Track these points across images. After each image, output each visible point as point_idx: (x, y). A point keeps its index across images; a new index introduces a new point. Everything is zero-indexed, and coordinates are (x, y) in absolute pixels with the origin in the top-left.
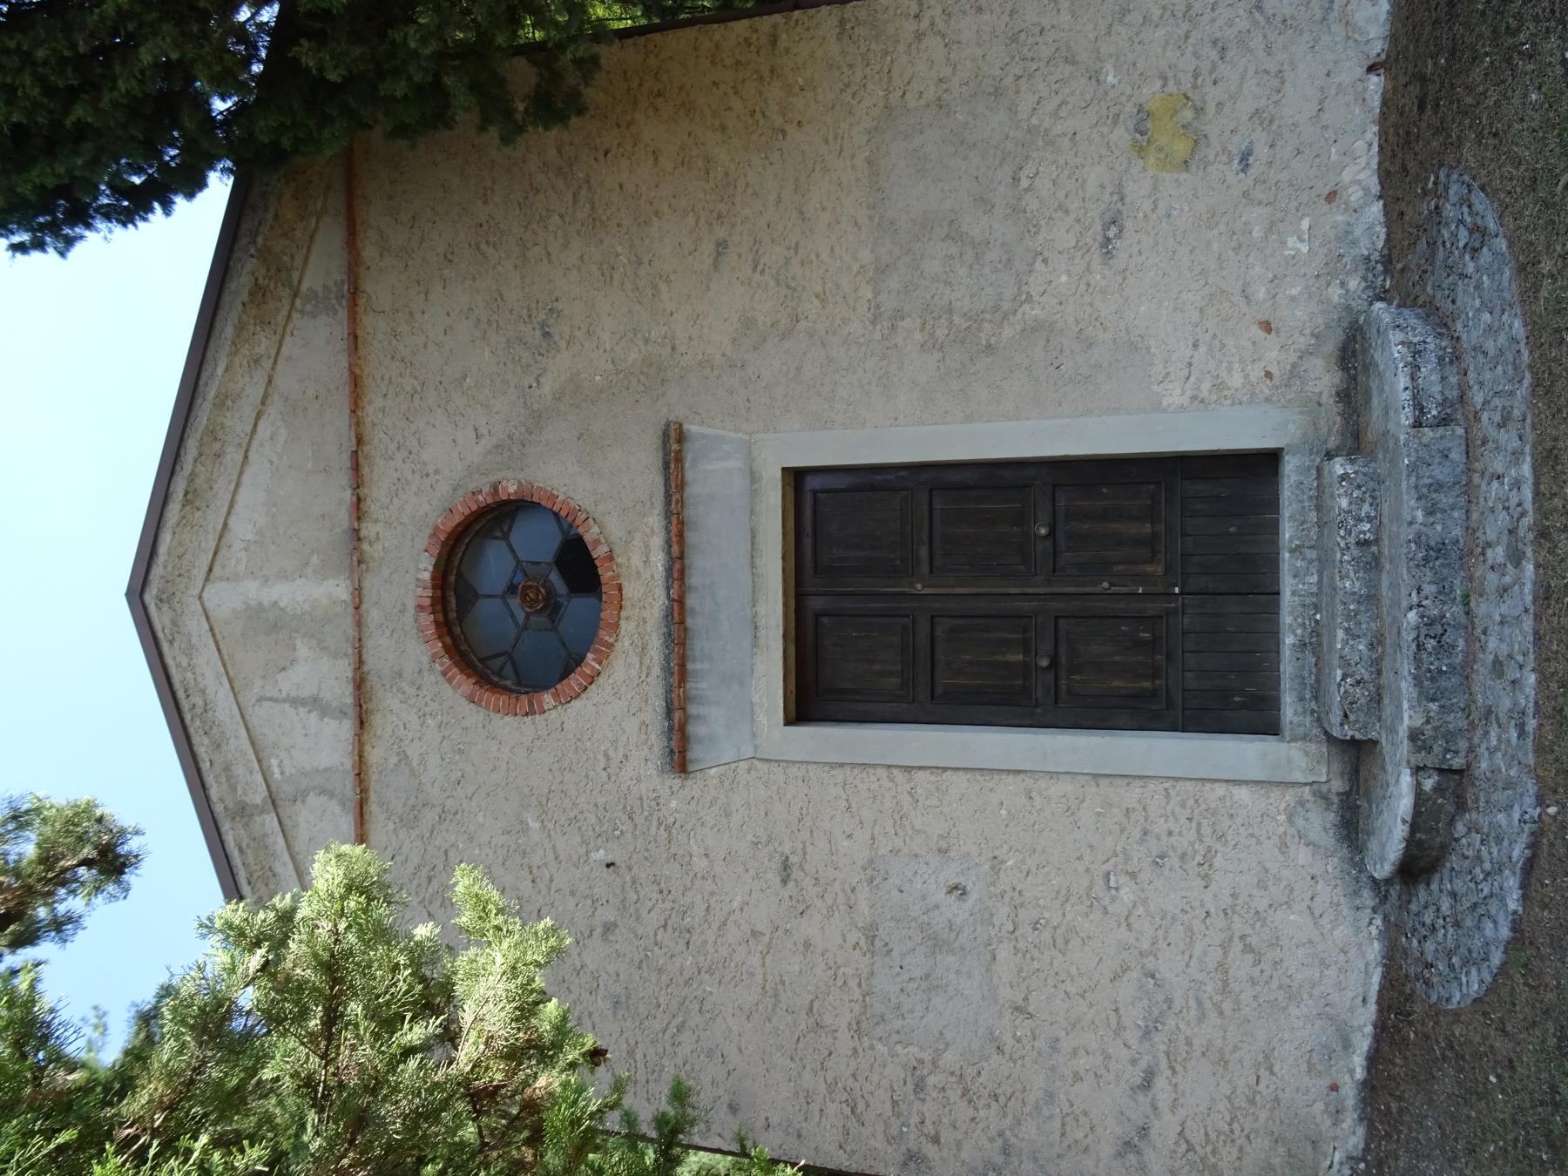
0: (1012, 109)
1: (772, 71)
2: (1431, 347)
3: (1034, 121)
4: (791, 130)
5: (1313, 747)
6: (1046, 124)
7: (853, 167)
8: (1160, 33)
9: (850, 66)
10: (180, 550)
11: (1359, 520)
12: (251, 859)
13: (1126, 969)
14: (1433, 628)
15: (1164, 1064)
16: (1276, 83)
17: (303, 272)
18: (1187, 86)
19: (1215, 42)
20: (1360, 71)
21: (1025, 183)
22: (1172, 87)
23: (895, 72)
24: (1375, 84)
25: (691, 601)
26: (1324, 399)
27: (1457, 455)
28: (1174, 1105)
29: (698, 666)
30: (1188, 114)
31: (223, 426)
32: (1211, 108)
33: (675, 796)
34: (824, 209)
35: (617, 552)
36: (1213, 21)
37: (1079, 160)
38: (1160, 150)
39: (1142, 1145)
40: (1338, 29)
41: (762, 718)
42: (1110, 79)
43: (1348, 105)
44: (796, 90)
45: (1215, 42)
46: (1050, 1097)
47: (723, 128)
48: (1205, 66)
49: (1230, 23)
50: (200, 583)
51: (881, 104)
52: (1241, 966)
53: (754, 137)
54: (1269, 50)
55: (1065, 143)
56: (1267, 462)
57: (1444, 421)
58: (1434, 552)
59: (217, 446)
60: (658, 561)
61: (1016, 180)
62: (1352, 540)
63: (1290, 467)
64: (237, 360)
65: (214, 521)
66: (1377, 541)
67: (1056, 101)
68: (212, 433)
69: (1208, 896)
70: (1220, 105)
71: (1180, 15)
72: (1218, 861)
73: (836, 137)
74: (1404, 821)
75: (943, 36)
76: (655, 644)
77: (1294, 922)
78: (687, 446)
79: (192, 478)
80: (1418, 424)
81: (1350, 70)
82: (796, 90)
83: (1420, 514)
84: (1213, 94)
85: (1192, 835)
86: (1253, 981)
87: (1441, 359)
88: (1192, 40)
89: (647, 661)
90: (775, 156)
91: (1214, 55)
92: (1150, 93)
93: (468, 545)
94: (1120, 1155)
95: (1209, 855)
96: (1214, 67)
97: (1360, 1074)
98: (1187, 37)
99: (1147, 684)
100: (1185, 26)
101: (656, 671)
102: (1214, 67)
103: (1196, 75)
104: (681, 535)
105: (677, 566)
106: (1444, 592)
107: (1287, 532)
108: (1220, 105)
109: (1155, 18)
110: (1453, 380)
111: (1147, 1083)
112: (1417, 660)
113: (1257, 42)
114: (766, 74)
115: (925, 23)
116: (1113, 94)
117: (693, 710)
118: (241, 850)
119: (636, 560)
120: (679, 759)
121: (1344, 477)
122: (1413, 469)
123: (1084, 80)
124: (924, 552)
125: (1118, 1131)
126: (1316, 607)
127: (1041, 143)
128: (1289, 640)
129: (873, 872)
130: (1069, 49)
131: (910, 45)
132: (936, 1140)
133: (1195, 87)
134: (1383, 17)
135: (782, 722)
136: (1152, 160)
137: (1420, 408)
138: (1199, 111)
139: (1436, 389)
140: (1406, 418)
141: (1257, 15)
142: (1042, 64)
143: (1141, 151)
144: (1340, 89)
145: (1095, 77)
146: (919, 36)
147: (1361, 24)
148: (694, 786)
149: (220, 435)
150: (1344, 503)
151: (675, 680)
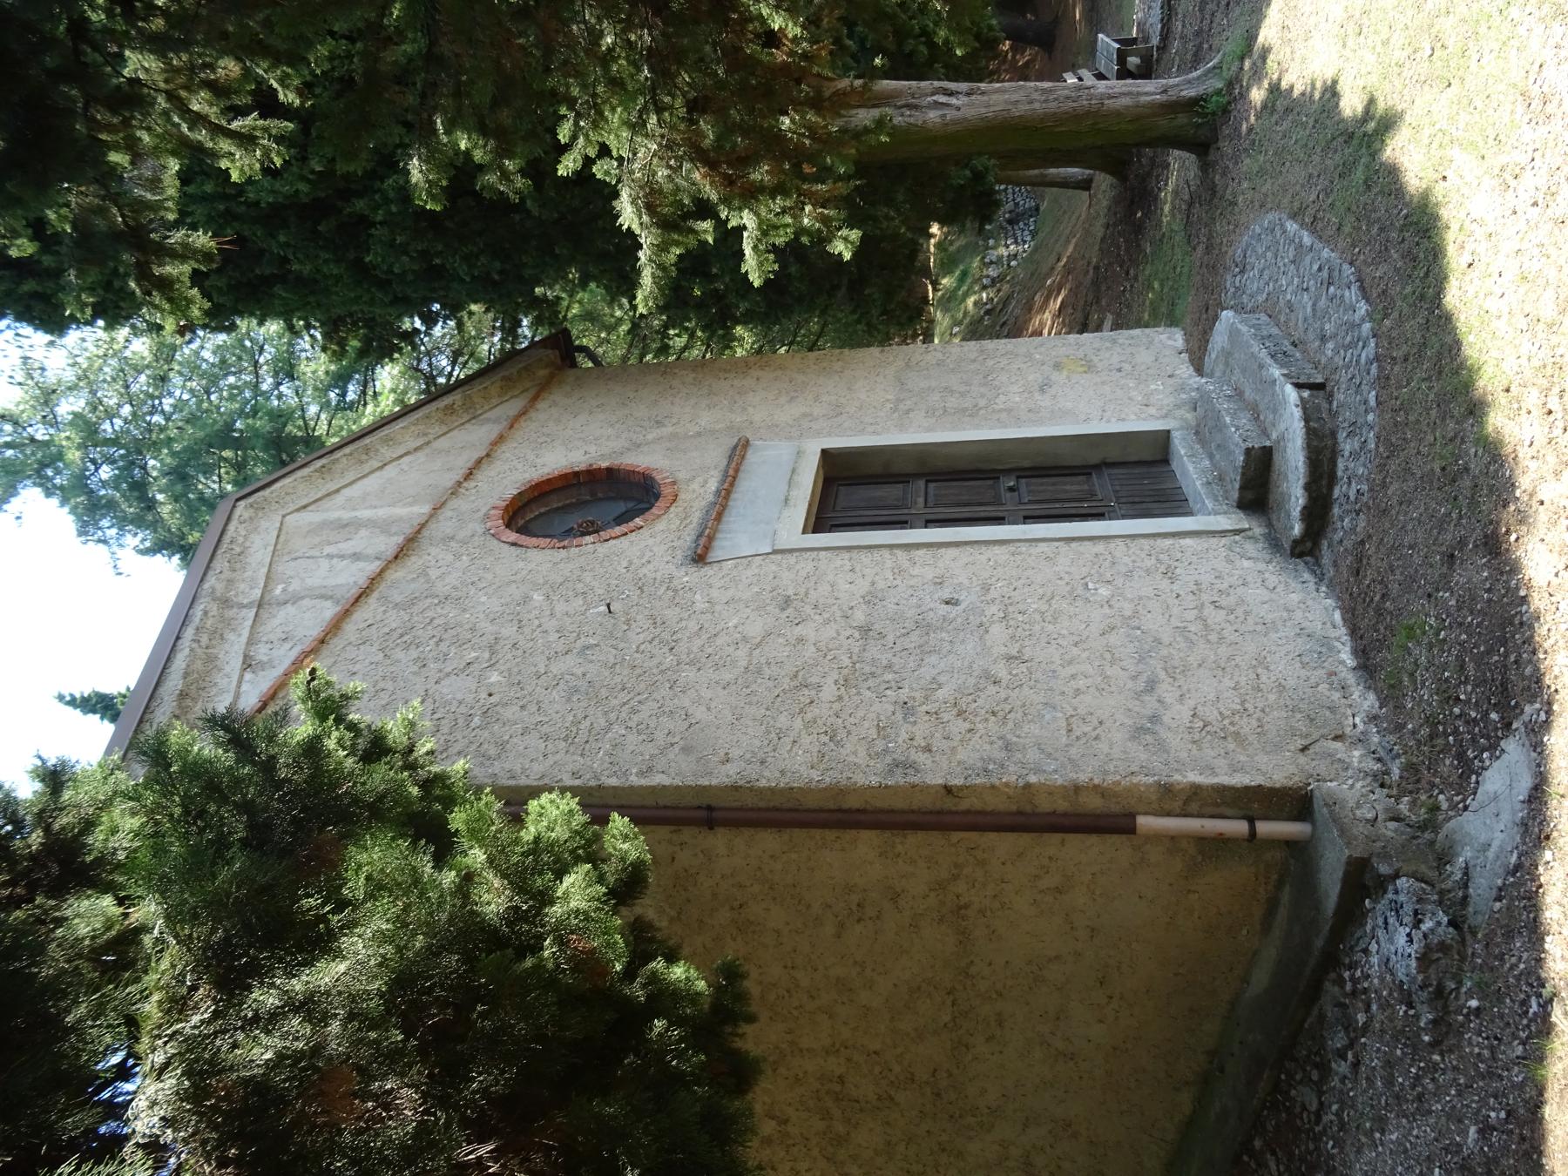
10: (291, 491)
17: (491, 409)
31: (377, 450)
39: (1157, 728)
50: (292, 507)
59: (364, 457)
63: (1181, 447)
64: (413, 428)
65: (332, 486)
68: (367, 450)
74: (1297, 406)
79: (333, 462)
93: (541, 515)
94: (1133, 738)
97: (1351, 662)
111: (1151, 686)
120: (700, 558)
125: (1129, 722)
135: (825, 447)
149: (372, 454)
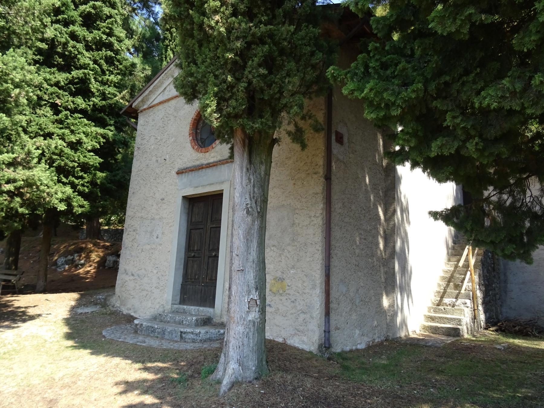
0: (289, 244)
1: (308, 174)
2: (198, 338)
3: (286, 251)
4: (293, 182)
5: (170, 310)
6: (285, 254)
7: (283, 201)
8: (300, 285)
9: (306, 197)
11: (186, 321)
12: (170, 72)
13: (146, 271)
14: (154, 331)
15: (134, 278)
16: (284, 315)
18: (287, 292)
19: (296, 300)
20: (283, 336)
21: (272, 248)
22: (288, 288)
23: (303, 211)
24: (280, 340)
25: (204, 170)
26: (222, 319)
27: (176, 339)
28: (129, 280)
29: (193, 174)
30: (281, 292)
32: (281, 298)
33: (174, 172)
34: (274, 193)
35: (214, 149)
36: (301, 300)
37: (275, 263)
38: (274, 284)
40: (293, 333)
41: (184, 191)
42: (292, 271)
43: (277, 332)
44: (303, 182)
45: (296, 300)
46: (132, 256)
47: (297, 161)
48: (290, 297)
49: (300, 304)
51: (296, 207)
52: (144, 293)
53: (293, 171)
54: (292, 314)
55: (280, 259)
56: (214, 307)
57: (181, 336)
58: (164, 332)
60: (212, 160)
61: (274, 246)
62: (183, 319)
66: (183, 324)
67: (289, 256)
69: (153, 288)
70: (281, 300)
71: (303, 291)
72: (158, 290)
73: (290, 195)
75: (309, 224)
76: (198, 163)
77: (149, 305)
78: (231, 163)
80: (181, 332)
81: (284, 334)
82: (303, 182)
83: (169, 330)
84: (284, 298)
85: (162, 285)
86: (143, 295)
87: (194, 339)
88: (297, 294)
89: (195, 161)
90: (288, 178)
91: (293, 300)
92: (287, 282)
95: (158, 288)
96: (290, 299)
98: (298, 293)
99: (189, 277)
100: (301, 292)
101: (194, 164)
102: (290, 299)
103: (289, 294)
104: (214, 166)
105: (208, 166)
106: (159, 333)
107: (201, 308)
108: (281, 300)
109: (304, 284)
110: (189, 341)
112: (151, 327)
113: (293, 311)
114: (308, 172)
115: (313, 219)
116: (288, 272)
117: (187, 174)
118: (170, 69)
119: (212, 155)
121: (193, 319)
122: (175, 330)
123: (293, 264)
124: (214, 226)
126: (189, 313)
127: (280, 253)
128: (185, 307)
129: (161, 219)
130: (301, 260)
131: (308, 214)
132: (128, 234)
133: (287, 294)
134: (295, 344)
136: (273, 282)
137: (185, 333)
138: (281, 295)
139: (187, 337)
140: (182, 330)
141: (300, 312)
142: (298, 253)
143: (275, 279)
144: (281, 331)
145: (293, 267)
146: (310, 217)
147: (294, 339)
148: (176, 175)
150: (189, 319)
151: (190, 169)
